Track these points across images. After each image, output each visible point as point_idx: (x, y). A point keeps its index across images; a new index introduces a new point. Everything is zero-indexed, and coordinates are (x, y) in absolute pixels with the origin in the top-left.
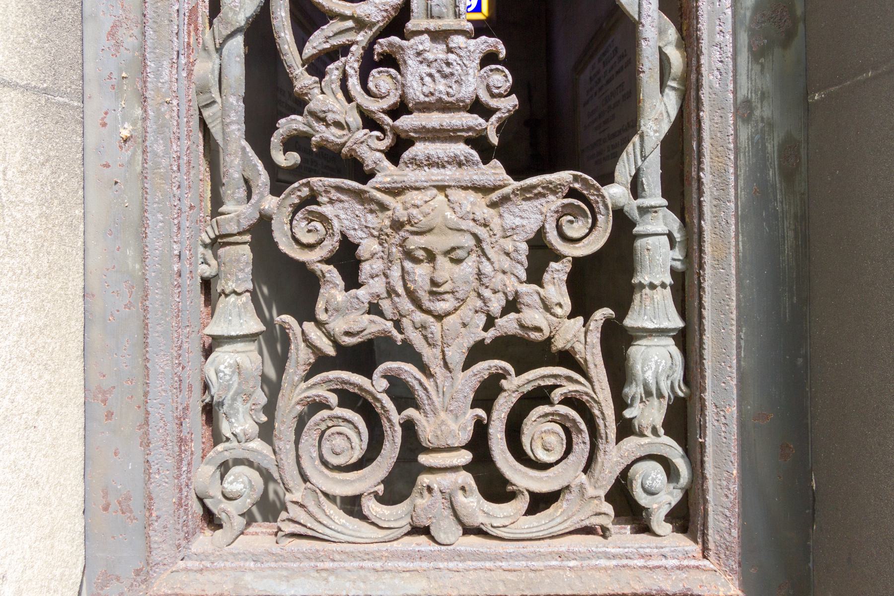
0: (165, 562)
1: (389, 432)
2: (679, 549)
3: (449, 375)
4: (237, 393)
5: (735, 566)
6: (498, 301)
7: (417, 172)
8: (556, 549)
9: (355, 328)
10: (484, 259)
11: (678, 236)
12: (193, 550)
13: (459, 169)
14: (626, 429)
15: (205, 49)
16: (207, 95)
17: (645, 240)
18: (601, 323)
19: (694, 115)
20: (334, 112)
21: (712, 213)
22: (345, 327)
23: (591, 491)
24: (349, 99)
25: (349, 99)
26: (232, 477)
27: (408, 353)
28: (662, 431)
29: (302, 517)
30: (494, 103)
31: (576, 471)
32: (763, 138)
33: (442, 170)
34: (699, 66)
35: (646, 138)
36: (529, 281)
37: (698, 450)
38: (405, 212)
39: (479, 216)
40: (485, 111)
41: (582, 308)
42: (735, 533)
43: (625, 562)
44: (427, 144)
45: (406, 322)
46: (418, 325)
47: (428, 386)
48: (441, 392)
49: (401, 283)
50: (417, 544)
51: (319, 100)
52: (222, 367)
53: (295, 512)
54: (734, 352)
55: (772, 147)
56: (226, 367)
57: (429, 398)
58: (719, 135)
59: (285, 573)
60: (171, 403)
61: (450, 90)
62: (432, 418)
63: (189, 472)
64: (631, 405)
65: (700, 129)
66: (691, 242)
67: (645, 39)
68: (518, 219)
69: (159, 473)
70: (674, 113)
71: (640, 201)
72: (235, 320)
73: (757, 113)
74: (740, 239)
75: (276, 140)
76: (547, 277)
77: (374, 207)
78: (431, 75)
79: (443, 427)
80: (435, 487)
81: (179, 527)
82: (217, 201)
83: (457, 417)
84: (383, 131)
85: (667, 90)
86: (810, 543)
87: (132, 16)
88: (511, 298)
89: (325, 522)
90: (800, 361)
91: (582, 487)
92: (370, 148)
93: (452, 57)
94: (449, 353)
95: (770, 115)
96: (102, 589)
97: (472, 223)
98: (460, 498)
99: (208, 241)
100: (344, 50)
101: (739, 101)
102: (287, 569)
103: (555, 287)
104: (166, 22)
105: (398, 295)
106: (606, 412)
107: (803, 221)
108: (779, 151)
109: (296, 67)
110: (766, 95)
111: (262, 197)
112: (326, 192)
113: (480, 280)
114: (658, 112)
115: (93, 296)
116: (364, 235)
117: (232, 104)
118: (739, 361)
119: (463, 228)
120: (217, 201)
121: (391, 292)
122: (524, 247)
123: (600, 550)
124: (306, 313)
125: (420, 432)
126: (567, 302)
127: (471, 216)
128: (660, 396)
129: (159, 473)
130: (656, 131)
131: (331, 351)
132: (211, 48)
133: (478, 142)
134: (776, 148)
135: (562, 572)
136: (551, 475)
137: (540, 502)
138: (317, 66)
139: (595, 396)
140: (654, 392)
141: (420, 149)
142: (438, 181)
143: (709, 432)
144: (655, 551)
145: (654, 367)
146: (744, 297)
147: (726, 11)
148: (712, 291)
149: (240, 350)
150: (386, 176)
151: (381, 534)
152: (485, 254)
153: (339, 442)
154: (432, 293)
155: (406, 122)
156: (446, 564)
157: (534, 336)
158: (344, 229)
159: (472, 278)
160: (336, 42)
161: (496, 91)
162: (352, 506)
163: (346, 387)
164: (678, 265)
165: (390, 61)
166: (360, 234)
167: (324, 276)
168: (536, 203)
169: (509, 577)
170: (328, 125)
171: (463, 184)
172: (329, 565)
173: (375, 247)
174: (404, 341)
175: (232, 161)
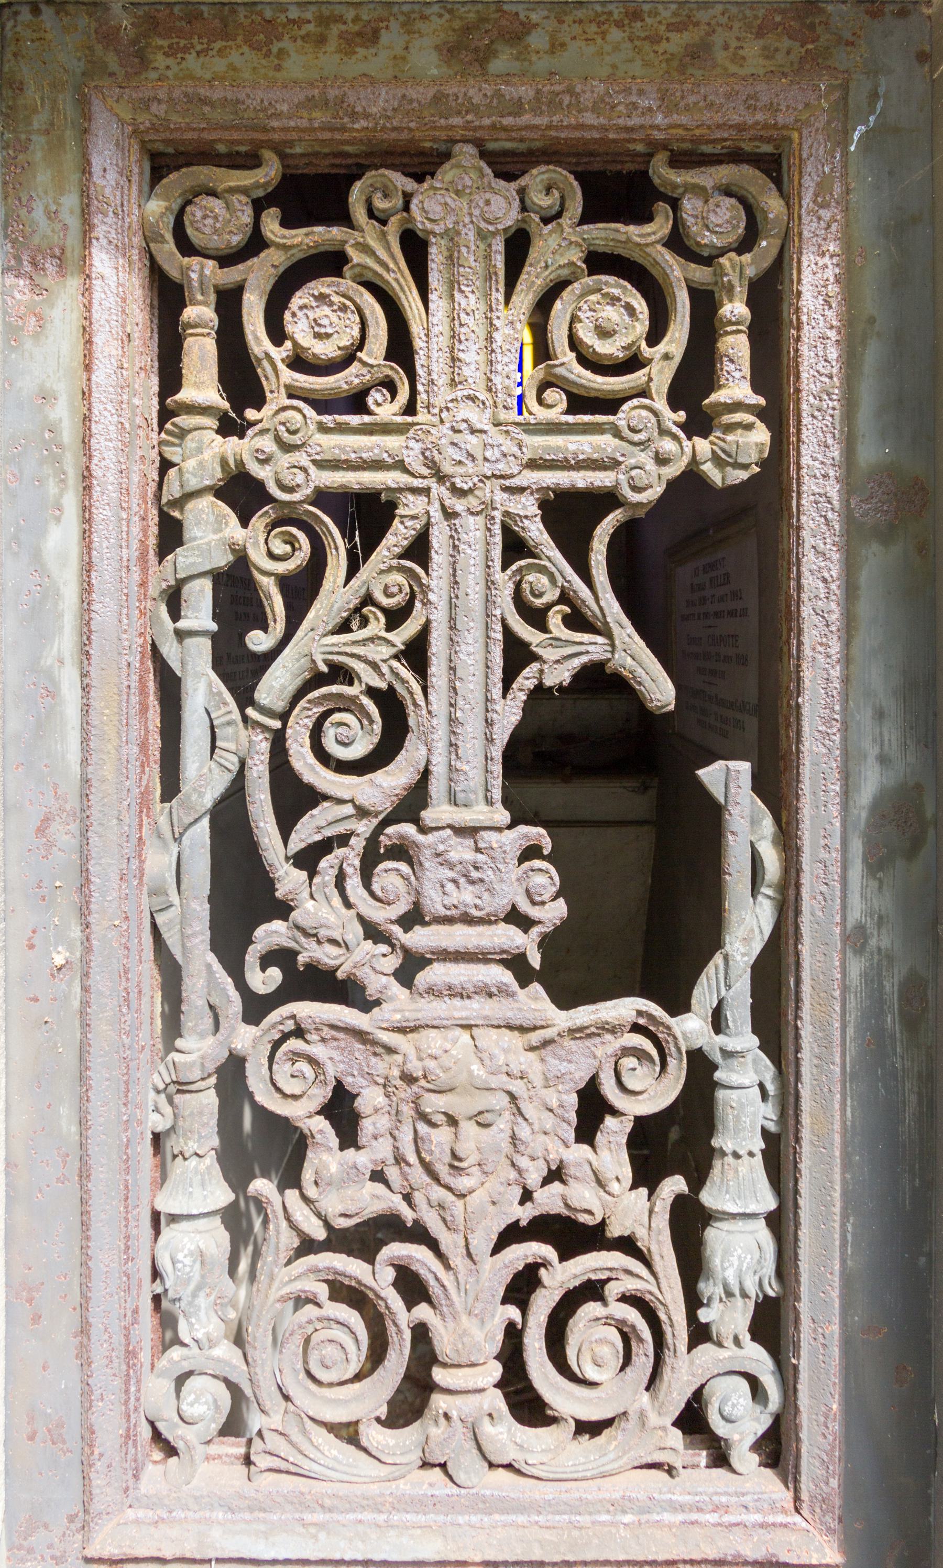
0: (110, 1510)
1: (395, 1339)
2: (765, 1496)
3: (474, 1267)
4: (199, 1288)
5: (834, 1525)
6: (537, 1170)
7: (434, 1003)
8: (607, 1496)
9: (352, 1210)
10: (520, 1120)
11: (771, 1088)
12: (143, 1490)
13: (489, 1000)
14: (700, 1334)
15: (159, 836)
16: (162, 898)
17: (728, 1092)
18: (670, 1201)
19: (791, 948)
20: (328, 927)
21: (812, 1074)
22: (340, 1208)
23: (653, 1419)
24: (348, 905)
25: (348, 905)
26: (193, 1397)
27: (419, 1234)
28: (746, 1337)
29: (282, 1447)
30: (534, 912)
31: (636, 1392)
32: (879, 975)
33: (467, 1002)
34: (798, 886)
35: (731, 963)
36: (579, 1139)
37: (791, 1371)
38: (419, 1064)
39: (515, 1069)
40: (523, 922)
41: (646, 1175)
42: (834, 1483)
43: (695, 1516)
44: (449, 965)
45: (418, 1197)
46: (435, 1203)
47: (446, 1283)
48: (463, 1290)
49: (413, 1148)
50: (431, 1485)
51: (307, 913)
52: (180, 1256)
53: (273, 1442)
54: (838, 1254)
55: (891, 986)
56: (185, 1256)
57: (447, 1297)
58: (821, 977)
59: (262, 1527)
60: (119, 1306)
61: (478, 902)
62: (451, 1324)
63: (138, 1390)
64: (708, 1305)
65: (798, 964)
66: (788, 1101)
67: (733, 833)
68: (565, 1064)
69: (102, 1400)
70: (768, 929)
71: (720, 1039)
72: (197, 1191)
73: (873, 942)
74: (849, 1102)
75: (252, 956)
76: (600, 1138)
77: (379, 1050)
78: (454, 881)
79: (465, 1340)
80: (454, 1414)
81: (127, 1466)
82: (173, 1025)
83: (483, 1322)
84: (393, 946)
85: (760, 898)
86: (931, 1491)
87: (68, 807)
88: (554, 1168)
89: (312, 1456)
90: (923, 1260)
91: (642, 1415)
92: (374, 969)
93: (481, 858)
94: (473, 1243)
95: (889, 946)
96: (25, 1539)
97: (505, 1078)
98: (487, 1429)
99: (161, 1086)
100: (343, 840)
101: (849, 926)
102: (265, 1521)
103: (612, 1153)
104: (115, 821)
105: (409, 1165)
106: (674, 1318)
107: (927, 1079)
108: (899, 991)
109: (278, 866)
110: (885, 920)
111: (233, 1029)
112: (317, 1029)
113: (515, 1145)
114: (748, 925)
115: (16, 1166)
116: (364, 1083)
117: (195, 910)
118: (843, 1261)
119: (493, 1086)
120: (173, 1025)
121: (399, 1160)
122: (573, 1099)
123: (663, 1497)
124: (291, 1178)
125: (435, 1342)
126: (627, 1173)
127: (505, 1069)
128: (744, 1295)
129: (102, 1400)
130: (743, 955)
131: (320, 1234)
132: (168, 835)
133: (516, 963)
134: (896, 988)
135: (614, 1530)
136: (603, 1395)
137: (589, 1428)
138: (308, 860)
139: (660, 1297)
140: (737, 1292)
141: (435, 974)
142: (461, 1019)
143: (804, 1352)
144: (734, 1499)
145: (736, 1263)
146: (852, 1179)
147: (834, 821)
148: (811, 1174)
149: (201, 1228)
150: (395, 1011)
151: (384, 1471)
152: (521, 1114)
153: (330, 1351)
154: (452, 1166)
155: (420, 938)
156: (467, 1517)
157: (583, 1218)
158: (338, 1075)
159: (506, 1146)
160: (329, 833)
161: (538, 899)
162: (348, 1433)
163: (339, 1278)
164: (772, 1127)
165: (401, 852)
166: (361, 1081)
167: (313, 1137)
168: (588, 1043)
169: (547, 1537)
170: (319, 942)
171: (495, 1023)
172: (319, 1517)
173: (381, 1100)
174: (416, 1222)
175: (194, 984)
